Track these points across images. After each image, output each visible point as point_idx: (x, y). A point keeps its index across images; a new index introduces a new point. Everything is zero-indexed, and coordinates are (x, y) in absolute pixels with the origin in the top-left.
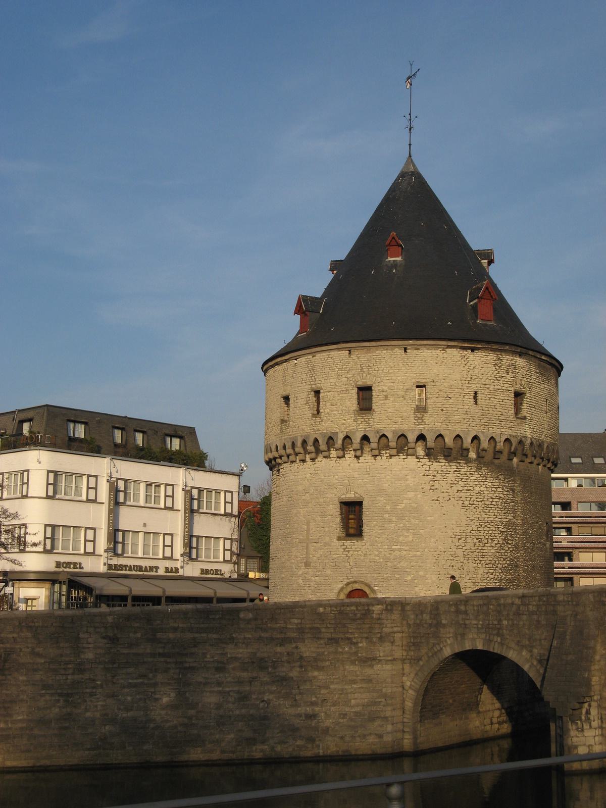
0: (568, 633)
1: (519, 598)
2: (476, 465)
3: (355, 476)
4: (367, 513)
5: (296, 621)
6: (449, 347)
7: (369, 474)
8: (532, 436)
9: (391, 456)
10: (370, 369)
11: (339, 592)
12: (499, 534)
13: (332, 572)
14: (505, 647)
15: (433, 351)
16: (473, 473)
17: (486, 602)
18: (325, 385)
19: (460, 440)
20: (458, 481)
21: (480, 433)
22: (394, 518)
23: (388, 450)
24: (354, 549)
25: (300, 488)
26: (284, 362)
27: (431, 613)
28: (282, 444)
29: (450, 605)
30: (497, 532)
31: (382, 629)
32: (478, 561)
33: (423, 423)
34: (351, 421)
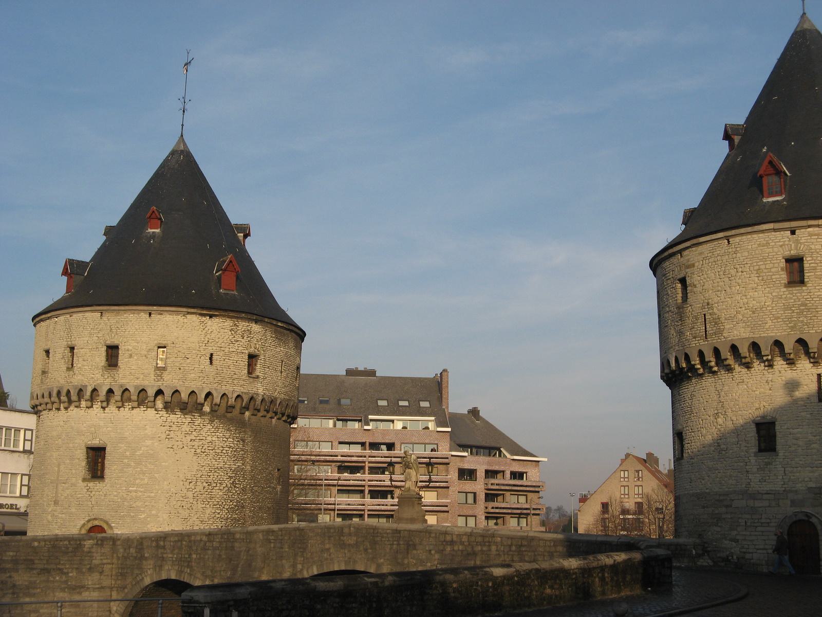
0: (240, 566)
1: (206, 535)
2: (209, 417)
3: (101, 425)
4: (109, 458)
5: (11, 554)
6: (188, 313)
7: (113, 423)
8: (264, 393)
9: (133, 408)
10: (118, 330)
11: (81, 528)
12: (227, 478)
13: (76, 510)
14: (193, 577)
15: (175, 317)
16: (206, 424)
17: (180, 538)
18: (78, 343)
19: (196, 396)
20: (192, 432)
21: (213, 390)
22: (132, 463)
23: (130, 402)
24: (96, 490)
25: (55, 433)
26: (48, 319)
27: (136, 547)
28: (42, 394)
29: (152, 541)
30: (226, 477)
31: (92, 561)
32: (207, 503)
33: (162, 380)
34: (99, 376)
